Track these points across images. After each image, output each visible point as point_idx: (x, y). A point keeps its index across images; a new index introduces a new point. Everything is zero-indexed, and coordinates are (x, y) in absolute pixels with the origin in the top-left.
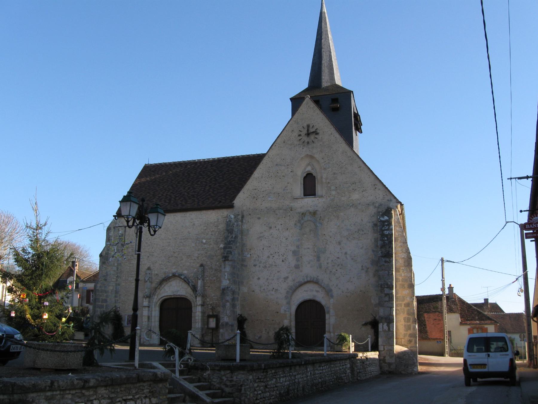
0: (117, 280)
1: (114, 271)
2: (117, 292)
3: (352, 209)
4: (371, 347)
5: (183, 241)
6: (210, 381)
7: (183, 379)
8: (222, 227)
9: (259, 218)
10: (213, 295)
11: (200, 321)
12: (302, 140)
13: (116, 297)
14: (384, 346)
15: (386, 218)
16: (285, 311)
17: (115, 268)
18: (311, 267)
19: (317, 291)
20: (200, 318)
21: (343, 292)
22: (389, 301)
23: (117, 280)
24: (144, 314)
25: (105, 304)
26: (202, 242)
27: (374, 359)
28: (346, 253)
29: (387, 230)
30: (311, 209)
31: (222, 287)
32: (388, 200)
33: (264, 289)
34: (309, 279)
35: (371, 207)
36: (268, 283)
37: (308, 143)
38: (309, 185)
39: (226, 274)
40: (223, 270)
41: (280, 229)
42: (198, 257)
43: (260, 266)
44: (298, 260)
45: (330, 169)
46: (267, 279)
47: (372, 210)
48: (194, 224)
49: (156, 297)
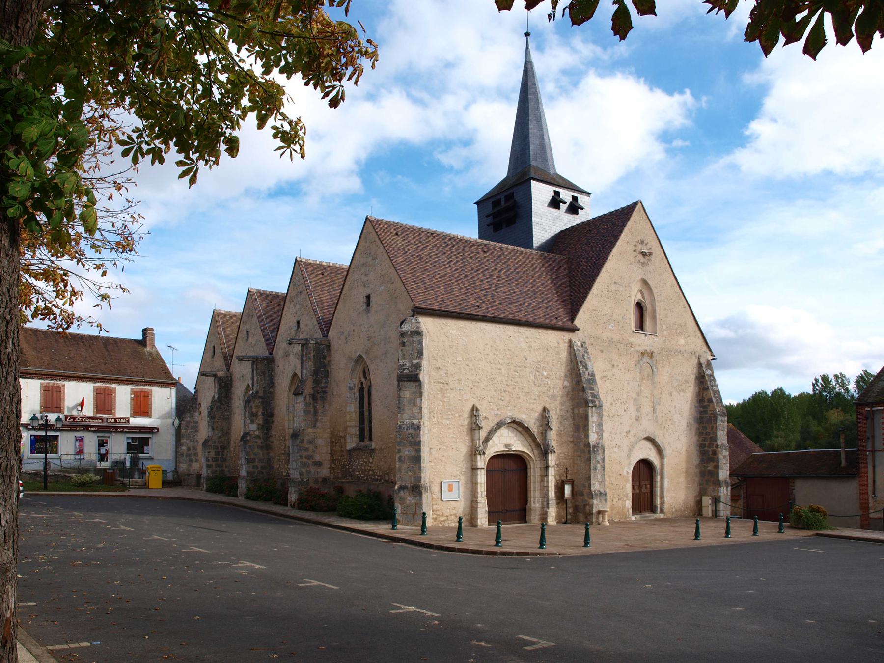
4: (141, 391)
5: (518, 369)
9: (602, 351)
26: (543, 375)
30: (648, 349)
37: (643, 264)
42: (539, 396)
48: (530, 347)
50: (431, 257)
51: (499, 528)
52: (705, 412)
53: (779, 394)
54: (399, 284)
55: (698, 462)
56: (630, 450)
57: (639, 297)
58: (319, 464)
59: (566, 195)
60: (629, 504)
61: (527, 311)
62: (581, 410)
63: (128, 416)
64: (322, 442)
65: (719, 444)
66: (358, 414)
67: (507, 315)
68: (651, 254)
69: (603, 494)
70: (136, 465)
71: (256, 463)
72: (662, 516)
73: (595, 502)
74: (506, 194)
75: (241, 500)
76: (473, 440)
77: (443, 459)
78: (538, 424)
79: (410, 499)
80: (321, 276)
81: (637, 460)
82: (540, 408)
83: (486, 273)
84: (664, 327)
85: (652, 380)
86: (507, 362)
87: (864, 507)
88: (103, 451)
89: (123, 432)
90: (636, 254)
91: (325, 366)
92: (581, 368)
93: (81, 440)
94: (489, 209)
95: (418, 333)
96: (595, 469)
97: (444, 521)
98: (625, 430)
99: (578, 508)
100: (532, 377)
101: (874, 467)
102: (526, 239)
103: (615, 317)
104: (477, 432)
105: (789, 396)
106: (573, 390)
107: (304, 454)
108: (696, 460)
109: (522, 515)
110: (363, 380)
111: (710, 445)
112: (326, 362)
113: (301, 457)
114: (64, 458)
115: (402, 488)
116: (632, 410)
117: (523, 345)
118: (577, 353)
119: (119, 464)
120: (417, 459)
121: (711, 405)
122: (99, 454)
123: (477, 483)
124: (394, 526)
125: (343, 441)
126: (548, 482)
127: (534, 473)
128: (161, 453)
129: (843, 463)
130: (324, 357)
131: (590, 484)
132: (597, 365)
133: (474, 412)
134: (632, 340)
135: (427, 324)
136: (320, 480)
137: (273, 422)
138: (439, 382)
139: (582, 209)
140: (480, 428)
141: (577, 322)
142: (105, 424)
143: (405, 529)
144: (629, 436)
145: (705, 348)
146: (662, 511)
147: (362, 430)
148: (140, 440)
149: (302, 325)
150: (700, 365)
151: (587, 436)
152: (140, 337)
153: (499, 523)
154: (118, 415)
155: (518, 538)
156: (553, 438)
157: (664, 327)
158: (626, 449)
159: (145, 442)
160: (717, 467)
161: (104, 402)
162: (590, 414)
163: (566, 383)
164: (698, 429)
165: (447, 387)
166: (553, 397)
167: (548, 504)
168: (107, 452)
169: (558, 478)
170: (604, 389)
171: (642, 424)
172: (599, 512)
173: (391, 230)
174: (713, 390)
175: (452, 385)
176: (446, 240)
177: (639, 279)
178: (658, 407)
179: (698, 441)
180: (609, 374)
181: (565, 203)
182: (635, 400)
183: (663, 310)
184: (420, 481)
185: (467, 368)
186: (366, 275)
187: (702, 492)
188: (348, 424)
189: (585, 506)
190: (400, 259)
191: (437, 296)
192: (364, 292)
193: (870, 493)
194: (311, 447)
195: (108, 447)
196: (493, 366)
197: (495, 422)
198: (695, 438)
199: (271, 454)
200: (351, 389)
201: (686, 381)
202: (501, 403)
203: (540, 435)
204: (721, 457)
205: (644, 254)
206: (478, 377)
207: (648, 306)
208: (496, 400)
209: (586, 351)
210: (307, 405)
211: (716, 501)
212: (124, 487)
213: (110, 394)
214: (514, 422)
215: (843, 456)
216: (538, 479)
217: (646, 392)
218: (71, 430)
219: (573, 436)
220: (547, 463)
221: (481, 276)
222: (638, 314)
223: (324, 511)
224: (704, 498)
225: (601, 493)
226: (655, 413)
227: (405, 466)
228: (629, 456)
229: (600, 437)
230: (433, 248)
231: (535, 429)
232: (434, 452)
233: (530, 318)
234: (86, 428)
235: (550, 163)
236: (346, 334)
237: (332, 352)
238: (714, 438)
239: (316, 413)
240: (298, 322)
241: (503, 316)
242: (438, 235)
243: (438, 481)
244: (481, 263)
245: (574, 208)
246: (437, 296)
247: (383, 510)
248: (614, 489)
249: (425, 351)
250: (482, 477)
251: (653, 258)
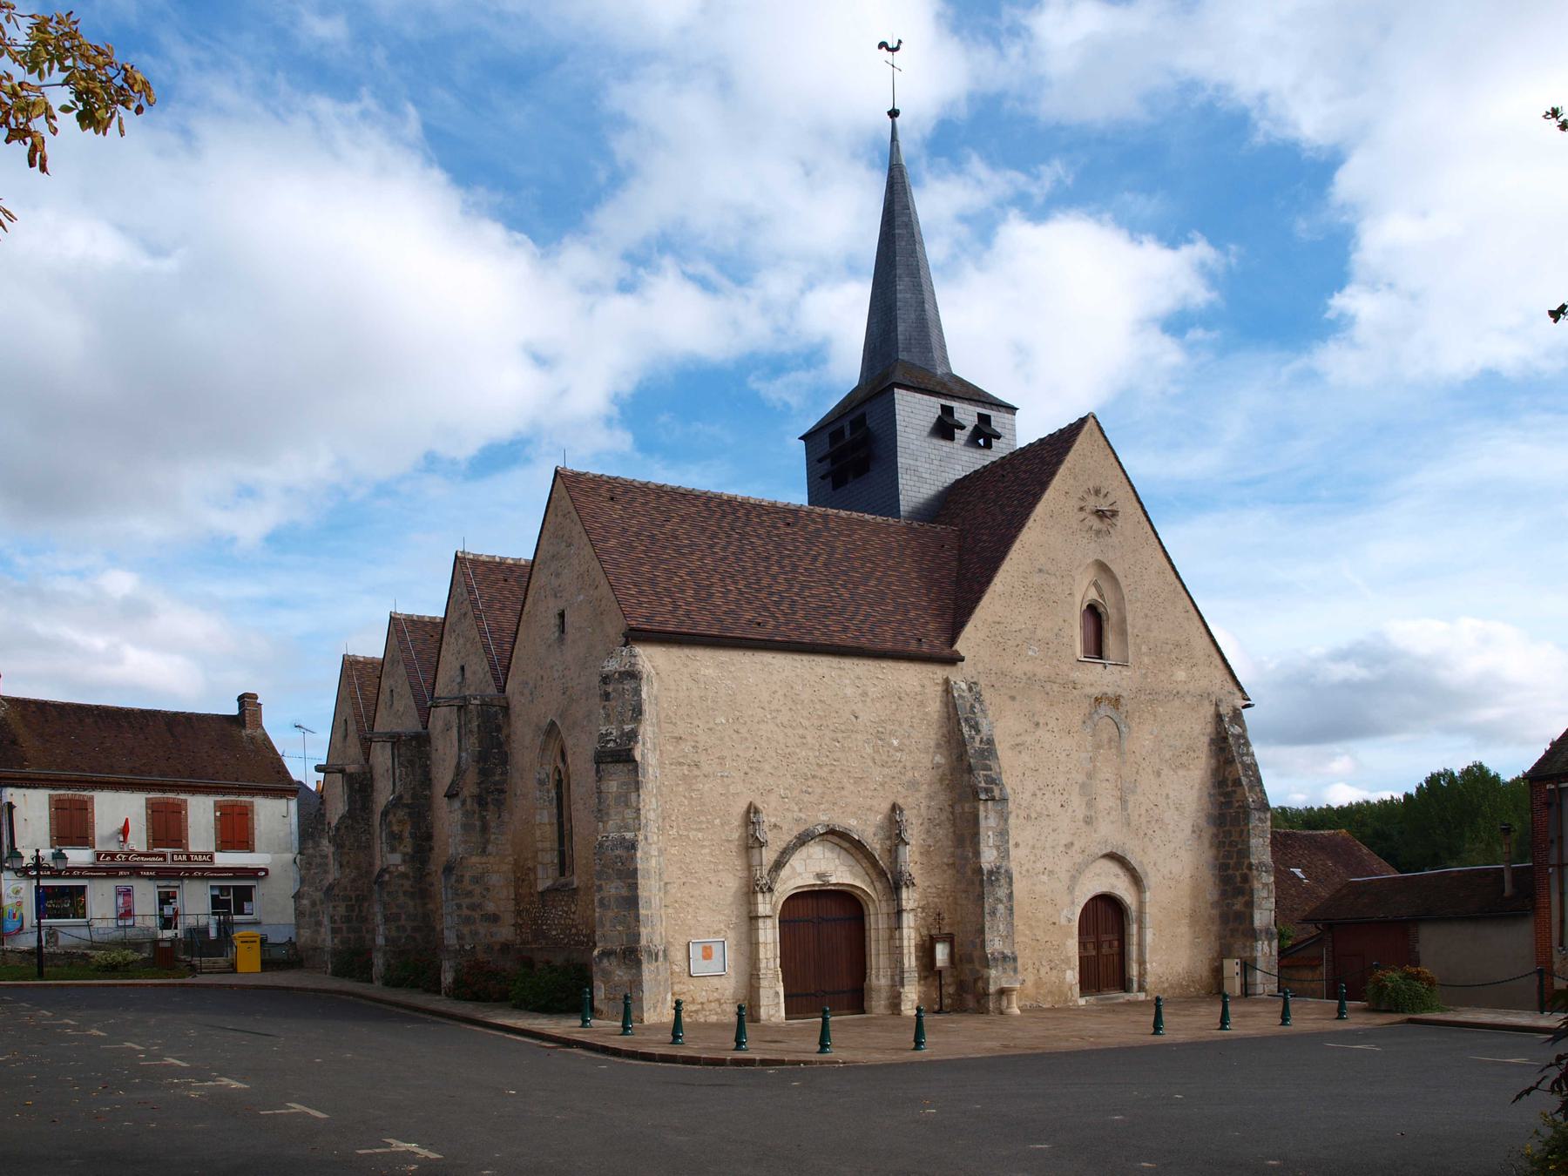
4: (233, 806)
9: (1013, 698)
19: (1117, 876)
26: (891, 745)
27: (947, 951)
30: (1110, 691)
37: (1098, 532)
48: (865, 694)
50: (676, 538)
51: (825, 1021)
52: (1229, 804)
53: (1478, 777)
54: (605, 589)
55: (1216, 897)
56: (1073, 879)
57: (1093, 595)
58: (494, 918)
59: (966, 414)
60: (1072, 976)
61: (859, 630)
62: (967, 807)
63: (212, 849)
64: (499, 880)
65: (1254, 861)
66: (556, 827)
67: (818, 637)
68: (1114, 514)
69: (1008, 960)
70: (227, 934)
71: (403, 922)
72: (1142, 996)
73: (993, 973)
74: (852, 417)
75: (376, 989)
76: (749, 867)
77: (692, 901)
78: (881, 835)
79: (620, 974)
80: (502, 584)
81: (1090, 896)
82: (885, 806)
83: (786, 562)
84: (1144, 649)
85: (1119, 748)
86: (817, 723)
87: (1544, 973)
88: (168, 911)
89: (202, 878)
90: (1082, 515)
91: (500, 745)
92: (965, 729)
93: (127, 893)
94: (825, 447)
95: (633, 675)
96: (993, 913)
97: (696, 1012)
98: (1063, 842)
99: (962, 984)
100: (869, 750)
101: (1562, 894)
102: (888, 501)
103: (1040, 633)
104: (756, 852)
105: (1497, 776)
106: (953, 770)
107: (466, 902)
108: (1211, 893)
109: (857, 1000)
110: (561, 765)
111: (1238, 865)
112: (502, 737)
113: (459, 906)
114: (97, 924)
115: (606, 954)
116: (1077, 803)
117: (849, 691)
118: (959, 702)
119: (198, 933)
120: (631, 902)
121: (1239, 791)
122: (161, 916)
123: (757, 943)
124: (585, 1021)
125: (532, 877)
126: (901, 939)
127: (877, 923)
128: (274, 910)
130: (499, 729)
131: (983, 941)
132: (1002, 725)
133: (751, 816)
135: (651, 659)
136: (497, 947)
137: (431, 849)
138: (681, 764)
139: (998, 437)
140: (762, 845)
141: (961, 646)
142: (168, 864)
143: (605, 1028)
144: (1072, 852)
145: (1230, 685)
146: (1141, 988)
147: (562, 854)
148: (235, 893)
149: (468, 674)
150: (1219, 717)
151: (977, 854)
152: (233, 710)
153: (825, 1012)
154: (192, 849)
155: (854, 1043)
156: (911, 859)
157: (1144, 649)
158: (1065, 877)
159: (245, 895)
160: (1250, 905)
161: (166, 826)
162: (982, 814)
163: (939, 759)
164: (1216, 836)
165: (696, 772)
166: (913, 785)
167: (902, 979)
168: (176, 914)
169: (925, 932)
170: (1012, 767)
171: (1090, 828)
172: (1002, 992)
173: (603, 491)
174: (1243, 763)
175: (706, 769)
176: (712, 505)
177: (1090, 561)
178: (1131, 799)
179: (1216, 858)
180: (1029, 739)
181: (962, 428)
182: (1083, 786)
183: (1138, 616)
184: (638, 941)
185: (735, 736)
186: (558, 575)
187: (1224, 952)
188: (539, 845)
189: (976, 981)
190: (613, 542)
191: (677, 607)
192: (553, 607)
193: (1555, 943)
194: (478, 889)
195: (178, 904)
196: (789, 731)
197: (795, 833)
198: (1208, 854)
199: (431, 906)
200: (541, 783)
201: (1190, 748)
202: (806, 798)
203: (886, 856)
204: (1257, 885)
205: (1100, 514)
206: (759, 752)
207: (1110, 611)
208: (795, 793)
209: (978, 698)
210: (466, 814)
211: (1248, 966)
212: (194, 970)
213: (178, 811)
214: (832, 832)
215: (1507, 876)
216: (884, 934)
217: (1106, 772)
218: (108, 877)
219: (953, 855)
220: (899, 904)
221: (775, 569)
222: (1091, 627)
223: (495, 1001)
224: (1226, 962)
225: (1005, 957)
226: (1124, 809)
227: (610, 914)
228: (1071, 889)
229: (1004, 854)
230: (683, 521)
231: (875, 845)
232: (673, 889)
233: (864, 642)
234: (136, 872)
235: (937, 354)
236: (531, 684)
237: (513, 718)
238: (1244, 852)
239: (485, 829)
240: (462, 668)
241: (807, 639)
242: (697, 497)
243: (683, 941)
244: (777, 545)
245: (984, 434)
246: (677, 607)
247: (570, 994)
248: (1038, 951)
249: (646, 707)
250: (769, 935)
251: (1119, 521)
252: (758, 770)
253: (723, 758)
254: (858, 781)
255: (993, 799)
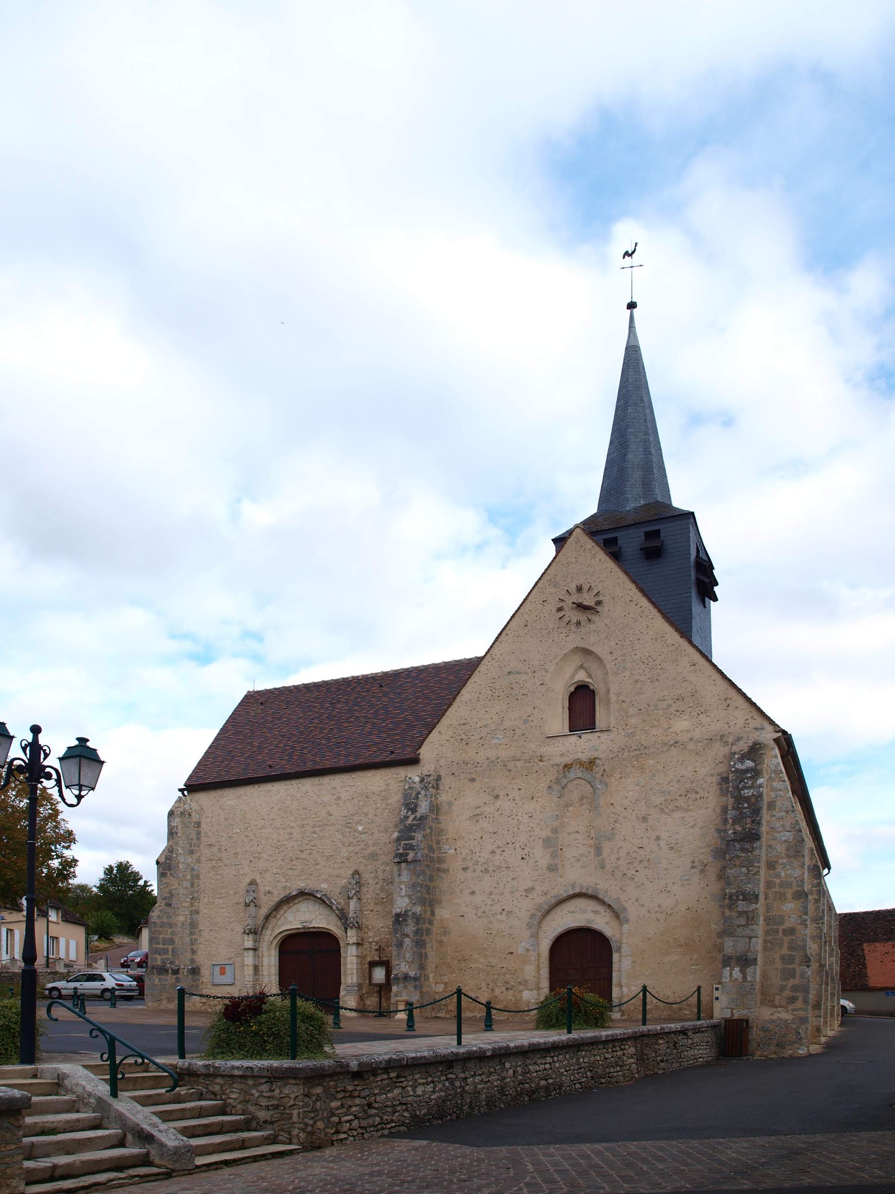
0: (192, 905)
1: (186, 888)
2: (193, 925)
3: (674, 751)
5: (317, 829)
6: (223, 1097)
7: (131, 1098)
8: (396, 799)
9: (473, 780)
10: (378, 925)
11: (355, 971)
12: (566, 619)
13: (191, 933)
14: (732, 1009)
15: (749, 764)
16: (528, 950)
17: (188, 884)
18: (582, 867)
19: (596, 912)
20: (355, 966)
21: (649, 912)
22: (747, 924)
23: (192, 905)
24: (246, 963)
25: (170, 947)
26: (356, 831)
28: (658, 838)
29: (749, 788)
30: (584, 757)
31: (394, 911)
32: (756, 729)
33: (484, 912)
34: (577, 890)
35: (717, 745)
36: (493, 900)
38: (582, 706)
39: (403, 886)
40: (397, 879)
41: (517, 798)
42: (348, 859)
43: (474, 871)
44: (554, 855)
45: (627, 674)
46: (491, 893)
47: (719, 751)
48: (339, 798)
49: (269, 932)
103: (507, 724)
129: (26, 1140)
134: (543, 750)
166: (373, 856)
178: (607, 847)
202: (290, 873)
206: (260, 847)
252: (259, 858)
253: (237, 854)
254: (329, 858)
255: (406, 861)
